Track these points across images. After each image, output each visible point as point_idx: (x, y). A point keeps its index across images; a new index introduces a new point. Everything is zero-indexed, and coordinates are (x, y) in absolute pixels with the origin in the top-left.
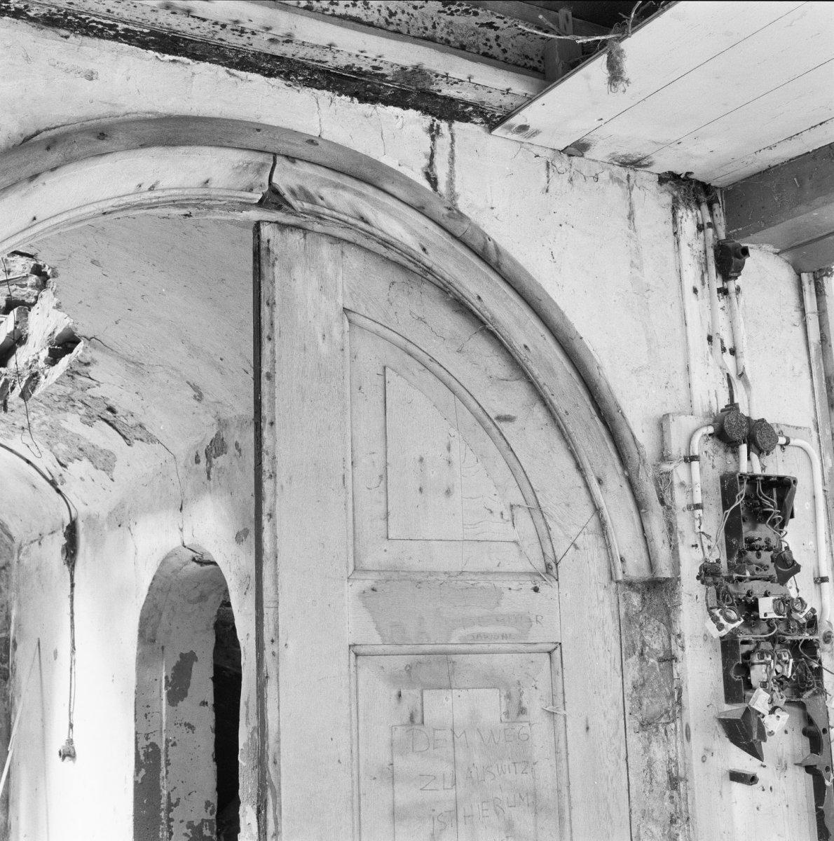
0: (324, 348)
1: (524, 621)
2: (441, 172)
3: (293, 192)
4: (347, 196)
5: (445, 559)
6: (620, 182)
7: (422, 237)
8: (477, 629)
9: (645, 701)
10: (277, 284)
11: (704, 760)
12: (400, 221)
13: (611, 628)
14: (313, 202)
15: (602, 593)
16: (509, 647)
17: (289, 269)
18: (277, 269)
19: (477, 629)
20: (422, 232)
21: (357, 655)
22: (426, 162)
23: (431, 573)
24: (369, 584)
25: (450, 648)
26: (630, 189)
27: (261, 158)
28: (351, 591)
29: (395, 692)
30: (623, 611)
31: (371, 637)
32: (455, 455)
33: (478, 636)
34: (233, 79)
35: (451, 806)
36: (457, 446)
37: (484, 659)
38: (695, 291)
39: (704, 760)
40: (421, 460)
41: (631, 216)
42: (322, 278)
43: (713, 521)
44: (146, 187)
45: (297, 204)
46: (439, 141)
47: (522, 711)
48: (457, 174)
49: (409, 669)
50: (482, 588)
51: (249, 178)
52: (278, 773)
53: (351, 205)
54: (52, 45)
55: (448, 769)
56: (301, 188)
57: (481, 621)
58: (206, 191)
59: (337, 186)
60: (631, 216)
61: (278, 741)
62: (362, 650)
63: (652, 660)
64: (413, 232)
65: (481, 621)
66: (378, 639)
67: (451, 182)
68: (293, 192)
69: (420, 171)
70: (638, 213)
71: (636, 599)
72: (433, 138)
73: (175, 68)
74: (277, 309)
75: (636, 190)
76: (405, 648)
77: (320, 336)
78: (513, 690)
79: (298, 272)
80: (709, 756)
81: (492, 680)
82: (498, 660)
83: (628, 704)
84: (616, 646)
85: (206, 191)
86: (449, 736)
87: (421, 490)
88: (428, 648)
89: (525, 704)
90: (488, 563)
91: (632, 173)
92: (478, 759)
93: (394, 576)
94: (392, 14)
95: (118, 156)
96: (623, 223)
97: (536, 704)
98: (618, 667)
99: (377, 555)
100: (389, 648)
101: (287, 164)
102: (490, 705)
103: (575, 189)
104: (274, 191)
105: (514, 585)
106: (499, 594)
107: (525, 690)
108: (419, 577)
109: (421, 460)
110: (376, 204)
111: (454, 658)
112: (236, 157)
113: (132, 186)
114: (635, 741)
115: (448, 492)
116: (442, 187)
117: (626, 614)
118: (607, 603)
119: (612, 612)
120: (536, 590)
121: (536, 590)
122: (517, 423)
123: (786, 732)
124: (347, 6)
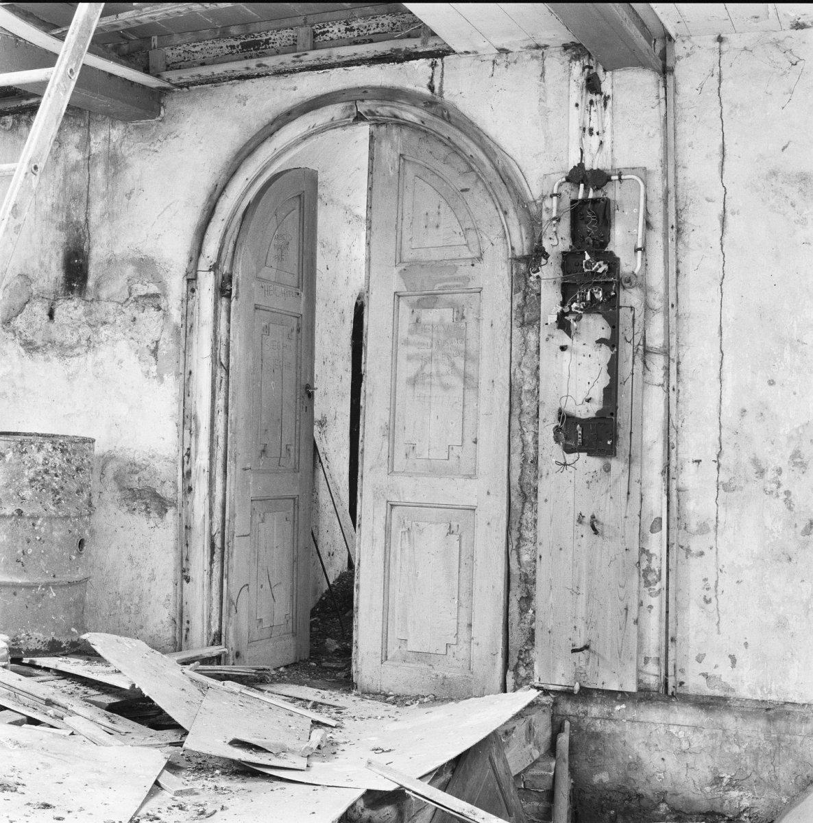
0: (392, 173)
1: (467, 279)
2: (436, 84)
3: (366, 113)
4: (388, 108)
5: (436, 255)
6: (537, 58)
7: (421, 117)
8: (445, 284)
9: (526, 314)
10: (375, 150)
11: (547, 340)
12: (411, 113)
13: (507, 280)
14: (374, 115)
15: (504, 265)
16: (460, 291)
17: (380, 143)
18: (375, 144)
19: (445, 284)
20: (420, 115)
21: (399, 296)
22: (429, 80)
23: (429, 261)
24: (403, 267)
25: (435, 292)
26: (543, 60)
27: (350, 104)
28: (396, 271)
29: (411, 310)
30: (514, 272)
31: (402, 288)
32: (441, 210)
33: (446, 286)
34: (346, 72)
35: (429, 355)
36: (443, 205)
37: (450, 296)
38: (577, 105)
39: (547, 340)
40: (427, 214)
41: (543, 75)
42: (392, 142)
43: (565, 227)
44: (311, 127)
45: (368, 118)
46: (436, 69)
47: (463, 317)
48: (445, 82)
49: (419, 301)
50: (449, 266)
51: (348, 112)
52: (367, 340)
53: (390, 112)
54: (282, 82)
55: (429, 341)
56: (369, 111)
57: (446, 280)
58: (332, 122)
59: (382, 106)
60: (543, 75)
61: (367, 329)
62: (401, 294)
63: (532, 295)
64: (416, 116)
65: (446, 280)
66: (405, 290)
67: (441, 87)
68: (366, 113)
69: (426, 86)
70: (547, 71)
71: (523, 267)
72: (433, 69)
73: (325, 75)
74: (375, 161)
75: (547, 59)
76: (417, 293)
77: (390, 169)
78: (460, 309)
79: (383, 144)
80: (550, 339)
81: (452, 305)
82: (456, 296)
83: (514, 315)
84: (509, 288)
85: (332, 122)
86: (431, 328)
87: (426, 227)
88: (426, 292)
89: (465, 315)
90: (454, 255)
91: (544, 51)
92: (442, 337)
93: (416, 264)
94: (394, 24)
95: (299, 119)
96: (536, 80)
97: (470, 317)
98: (509, 297)
99: (408, 255)
100: (410, 293)
101: (361, 103)
102: (448, 315)
103: (509, 70)
104: (358, 113)
105: (463, 264)
106: (456, 268)
107: (466, 309)
108: (423, 264)
109: (427, 214)
110: (399, 108)
111: (438, 296)
112: (340, 106)
113: (306, 128)
114: (516, 331)
115: (437, 227)
116: (437, 90)
117: (516, 274)
118: (506, 268)
119: (508, 274)
120: (473, 265)
121: (473, 265)
122: (471, 191)
123: (603, 328)
124: (374, 29)
